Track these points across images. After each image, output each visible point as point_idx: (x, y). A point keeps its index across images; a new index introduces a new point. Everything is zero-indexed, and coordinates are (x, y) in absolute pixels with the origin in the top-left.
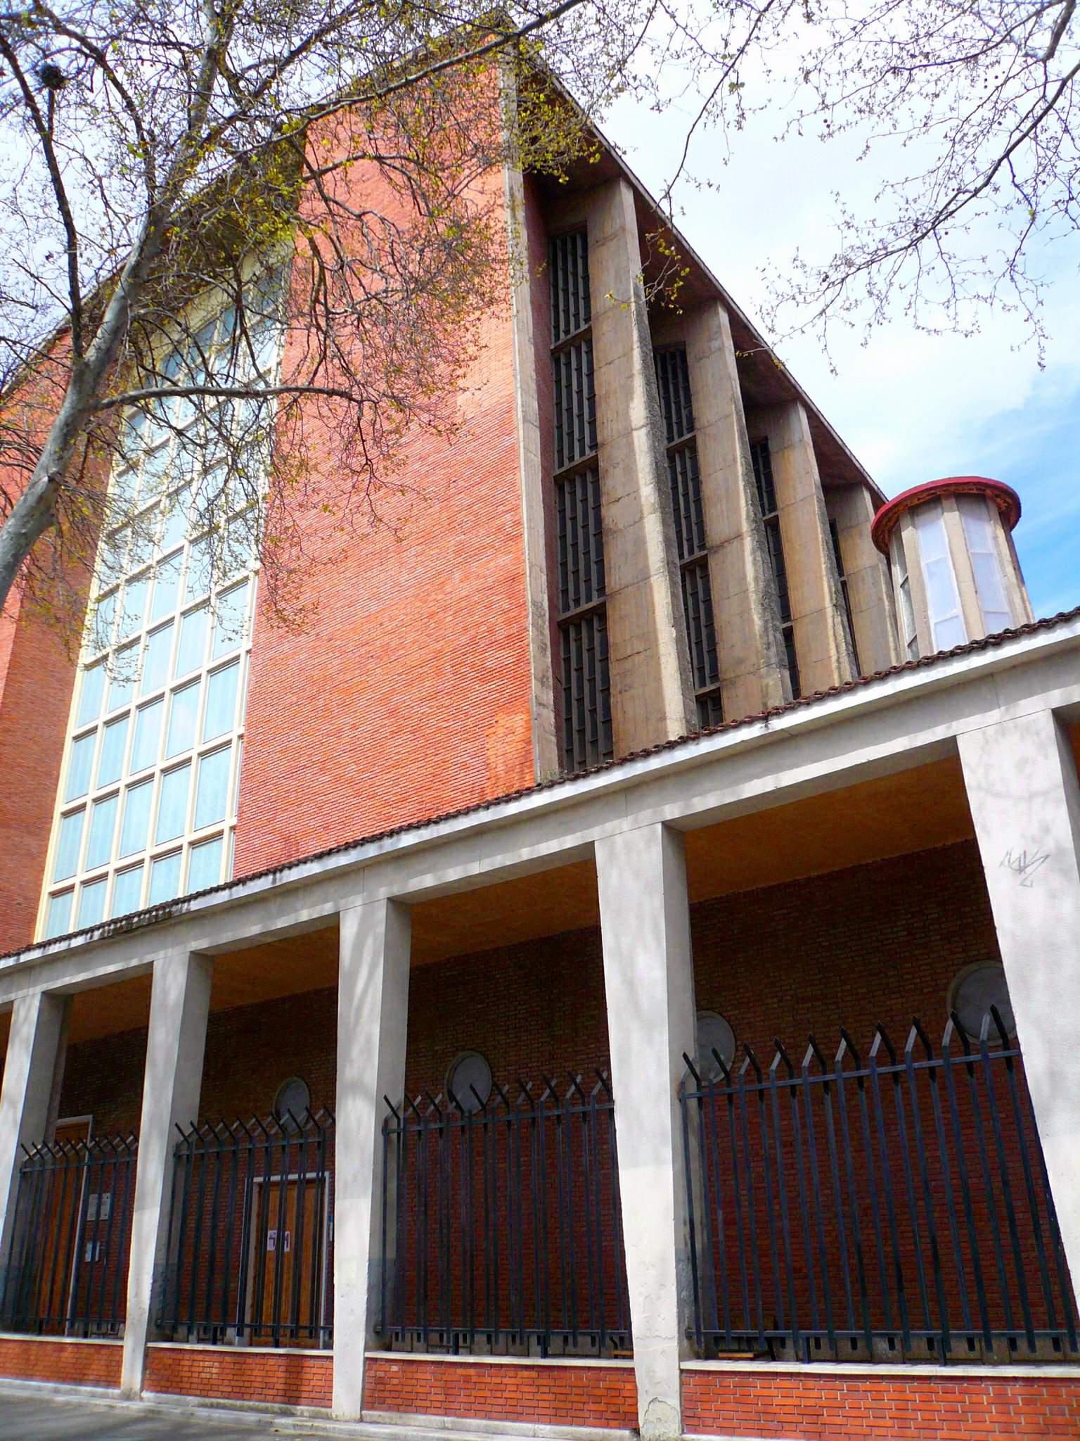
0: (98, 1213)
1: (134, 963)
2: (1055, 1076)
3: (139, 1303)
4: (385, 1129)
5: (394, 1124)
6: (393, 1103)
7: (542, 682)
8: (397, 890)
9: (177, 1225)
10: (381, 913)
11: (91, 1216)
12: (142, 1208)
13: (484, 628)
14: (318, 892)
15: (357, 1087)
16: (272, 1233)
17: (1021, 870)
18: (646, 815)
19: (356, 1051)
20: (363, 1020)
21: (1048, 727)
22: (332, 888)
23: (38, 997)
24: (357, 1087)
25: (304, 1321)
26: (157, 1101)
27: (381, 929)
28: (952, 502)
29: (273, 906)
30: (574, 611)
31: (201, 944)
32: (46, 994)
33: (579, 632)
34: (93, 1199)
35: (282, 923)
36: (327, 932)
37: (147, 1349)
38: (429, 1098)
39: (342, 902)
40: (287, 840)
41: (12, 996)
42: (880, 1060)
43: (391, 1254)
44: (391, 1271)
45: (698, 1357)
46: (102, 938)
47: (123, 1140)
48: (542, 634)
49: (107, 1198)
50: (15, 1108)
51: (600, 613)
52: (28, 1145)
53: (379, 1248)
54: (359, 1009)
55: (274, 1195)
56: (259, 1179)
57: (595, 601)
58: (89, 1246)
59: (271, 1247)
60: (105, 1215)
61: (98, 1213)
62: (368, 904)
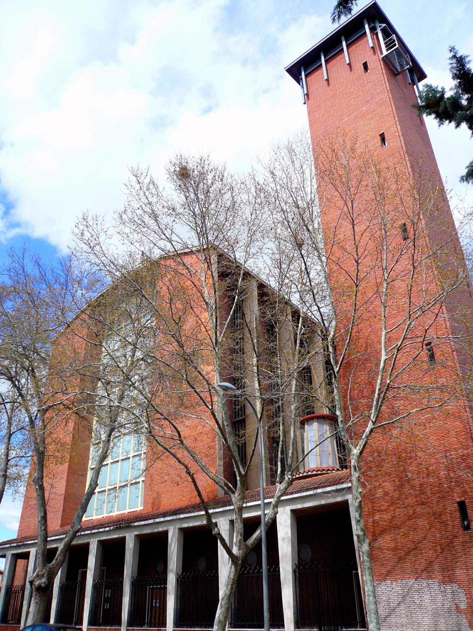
0: (108, 596)
1: (121, 536)
2: (285, 578)
3: (124, 619)
4: (177, 580)
5: (179, 579)
6: (179, 574)
7: (220, 459)
8: (180, 526)
9: (133, 600)
10: (177, 531)
11: (106, 596)
12: (125, 597)
13: (206, 442)
14: (164, 524)
15: (172, 571)
16: (154, 601)
17: (283, 540)
18: (227, 518)
19: (172, 563)
20: (173, 555)
21: (289, 513)
22: (166, 524)
23: (97, 541)
24: (172, 571)
25: (161, 622)
26: (128, 571)
27: (177, 535)
28: (316, 420)
29: (154, 526)
30: (238, 419)
31: (136, 533)
32: (98, 541)
33: (239, 425)
34: (107, 591)
35: (156, 530)
36: (166, 533)
37: (127, 629)
38: (186, 574)
39: (169, 527)
40: (157, 493)
41: (89, 540)
42: (257, 573)
43: (178, 607)
44: (178, 612)
45: (232, 628)
46: (113, 529)
47: (119, 580)
48: (220, 445)
49: (110, 591)
50: (92, 571)
51: (244, 420)
52: (95, 580)
53: (176, 606)
54: (172, 554)
55: (155, 591)
56: (151, 587)
57: (243, 417)
58: (106, 604)
59: (154, 605)
60: (109, 596)
61: (108, 596)
62: (174, 529)
